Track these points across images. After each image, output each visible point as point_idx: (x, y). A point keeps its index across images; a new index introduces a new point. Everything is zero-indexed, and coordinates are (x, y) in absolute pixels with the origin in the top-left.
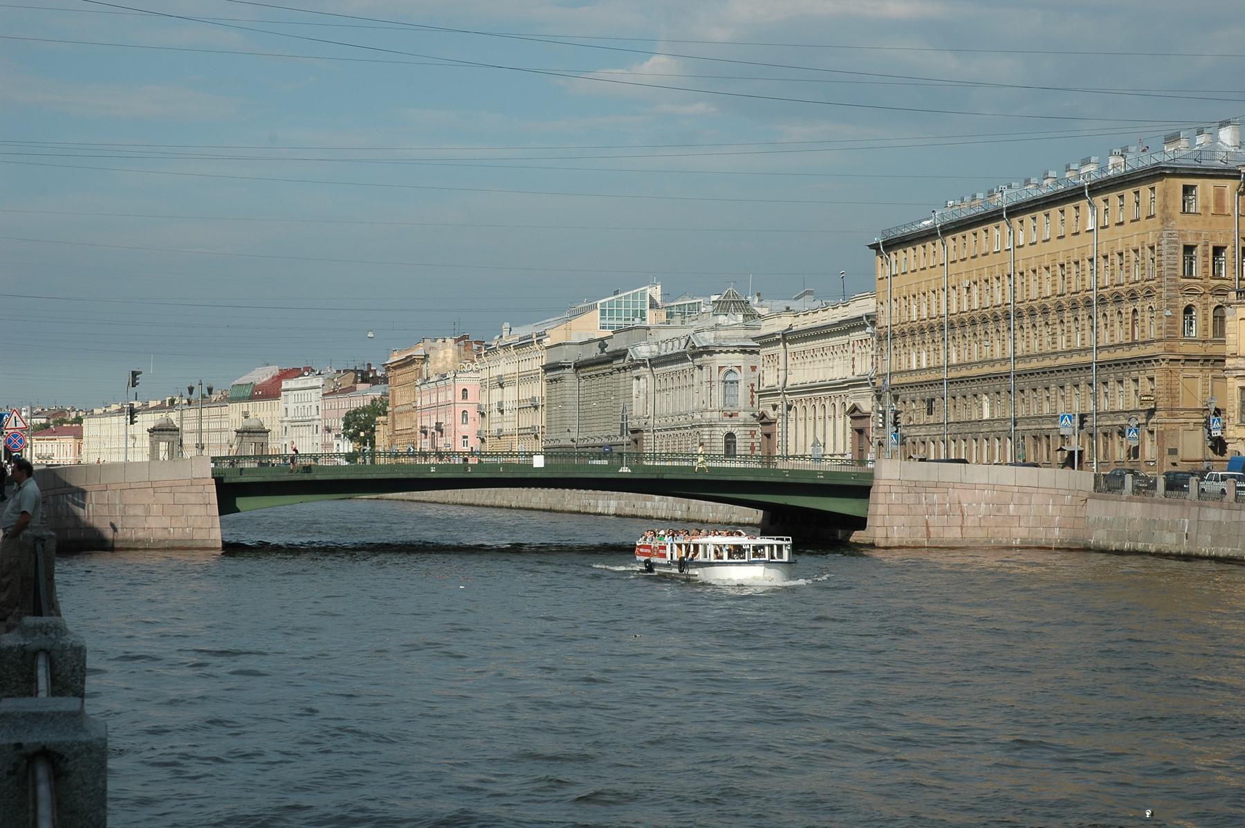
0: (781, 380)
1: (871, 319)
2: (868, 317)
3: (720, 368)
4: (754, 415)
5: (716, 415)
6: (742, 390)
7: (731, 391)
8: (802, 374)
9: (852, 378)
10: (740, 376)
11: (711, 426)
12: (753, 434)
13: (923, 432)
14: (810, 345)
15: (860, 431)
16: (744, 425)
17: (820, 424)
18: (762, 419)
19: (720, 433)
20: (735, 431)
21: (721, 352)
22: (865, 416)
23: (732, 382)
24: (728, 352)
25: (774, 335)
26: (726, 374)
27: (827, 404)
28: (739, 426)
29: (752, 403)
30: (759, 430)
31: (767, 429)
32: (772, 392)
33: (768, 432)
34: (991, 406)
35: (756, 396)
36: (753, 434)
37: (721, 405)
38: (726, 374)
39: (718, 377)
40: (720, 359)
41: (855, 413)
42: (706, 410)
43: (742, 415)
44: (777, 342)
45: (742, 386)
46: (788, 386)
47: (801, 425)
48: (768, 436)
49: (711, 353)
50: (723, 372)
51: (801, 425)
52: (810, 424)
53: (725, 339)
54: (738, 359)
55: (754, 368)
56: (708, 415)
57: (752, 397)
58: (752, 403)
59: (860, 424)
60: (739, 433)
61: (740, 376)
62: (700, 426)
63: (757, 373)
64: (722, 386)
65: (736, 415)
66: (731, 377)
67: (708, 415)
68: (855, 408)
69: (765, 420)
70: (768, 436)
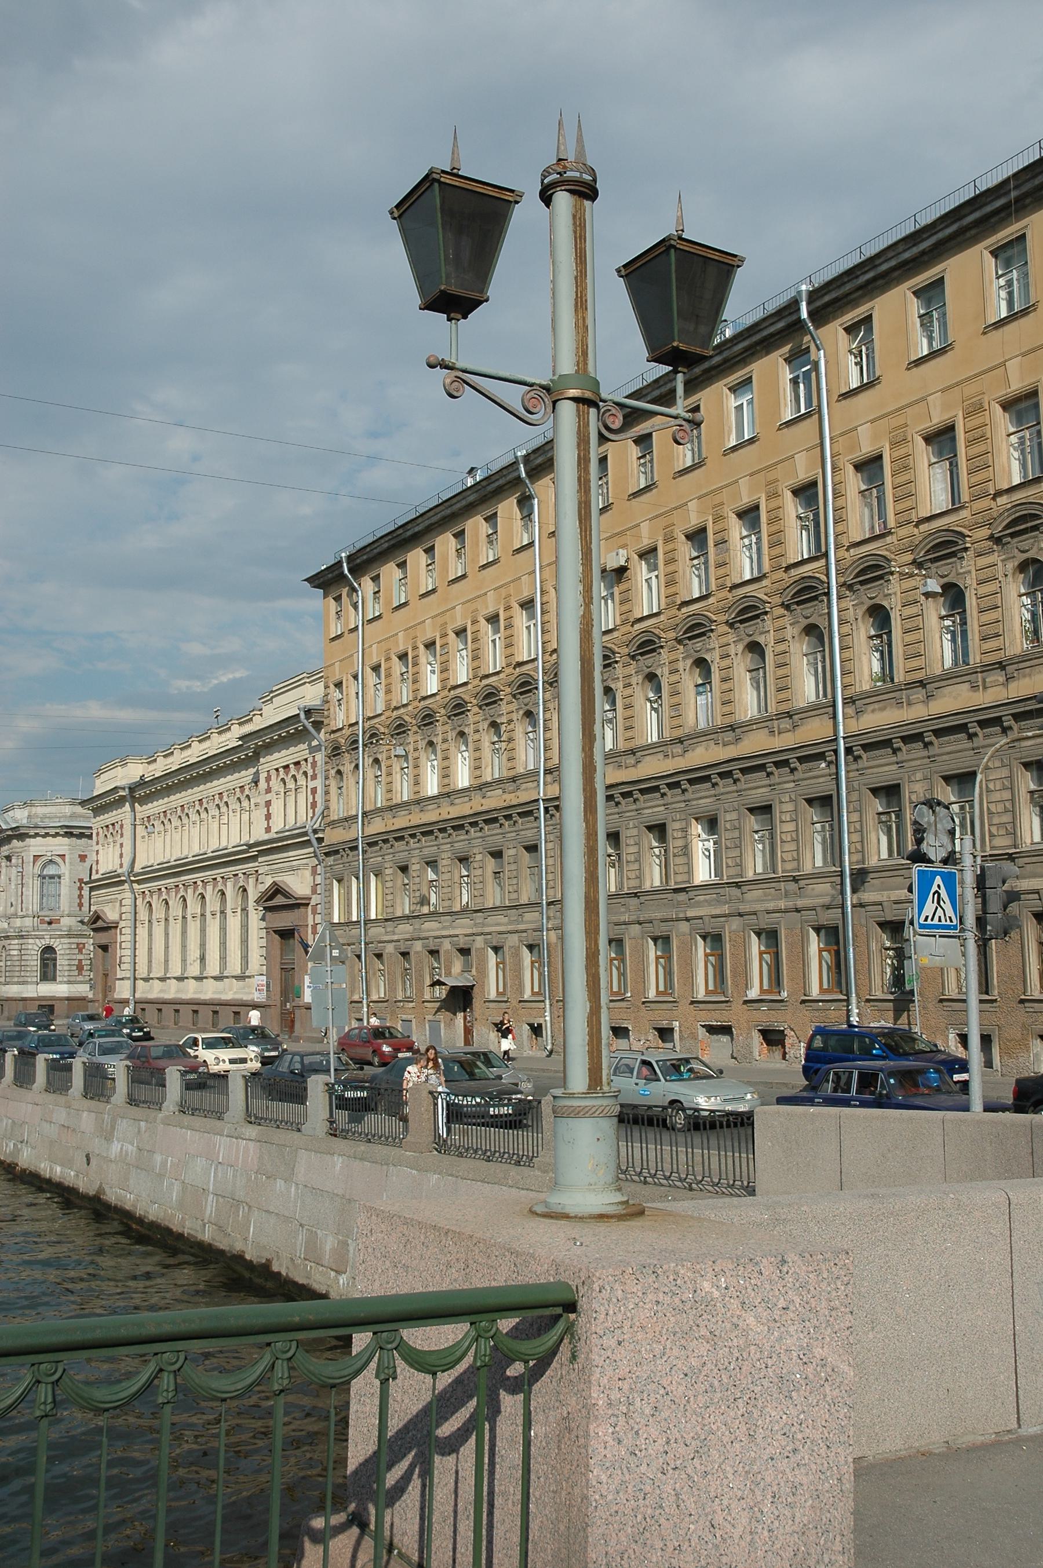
0: (127, 861)
1: (314, 718)
2: (308, 712)
3: (36, 857)
4: (82, 922)
5: (28, 922)
6: (66, 890)
7: (51, 888)
8: (158, 849)
9: (266, 837)
10: (64, 869)
11: (22, 937)
12: (80, 948)
13: (462, 927)
14: (177, 799)
15: (286, 934)
16: (69, 936)
17: (193, 928)
18: (98, 924)
19: (34, 947)
20: (55, 943)
21: (37, 835)
22: (299, 904)
23: (52, 877)
24: (47, 835)
25: (115, 789)
26: (44, 866)
27: (209, 892)
28: (61, 937)
29: (81, 905)
30: (89, 944)
31: (103, 938)
32: (113, 881)
33: (104, 942)
34: (63, 1025)
35: (86, 889)
36: (80, 948)
37: (37, 908)
38: (44, 866)
39: (30, 869)
40: (36, 846)
41: (276, 900)
42: (15, 915)
43: (66, 922)
44: (120, 802)
45: (65, 881)
46: (137, 869)
47: (158, 930)
48: (105, 948)
49: (22, 837)
50: (39, 863)
51: (158, 930)
52: (176, 928)
53: (44, 817)
54: (61, 845)
55: (83, 858)
56: (18, 923)
57: (81, 889)
58: (81, 905)
59: (284, 920)
60: (61, 946)
61: (64, 869)
62: (7, 938)
63: (87, 865)
64: (37, 883)
65: (58, 921)
66: (51, 870)
67: (18, 923)
68: (277, 890)
69: (100, 924)
70: (105, 948)
